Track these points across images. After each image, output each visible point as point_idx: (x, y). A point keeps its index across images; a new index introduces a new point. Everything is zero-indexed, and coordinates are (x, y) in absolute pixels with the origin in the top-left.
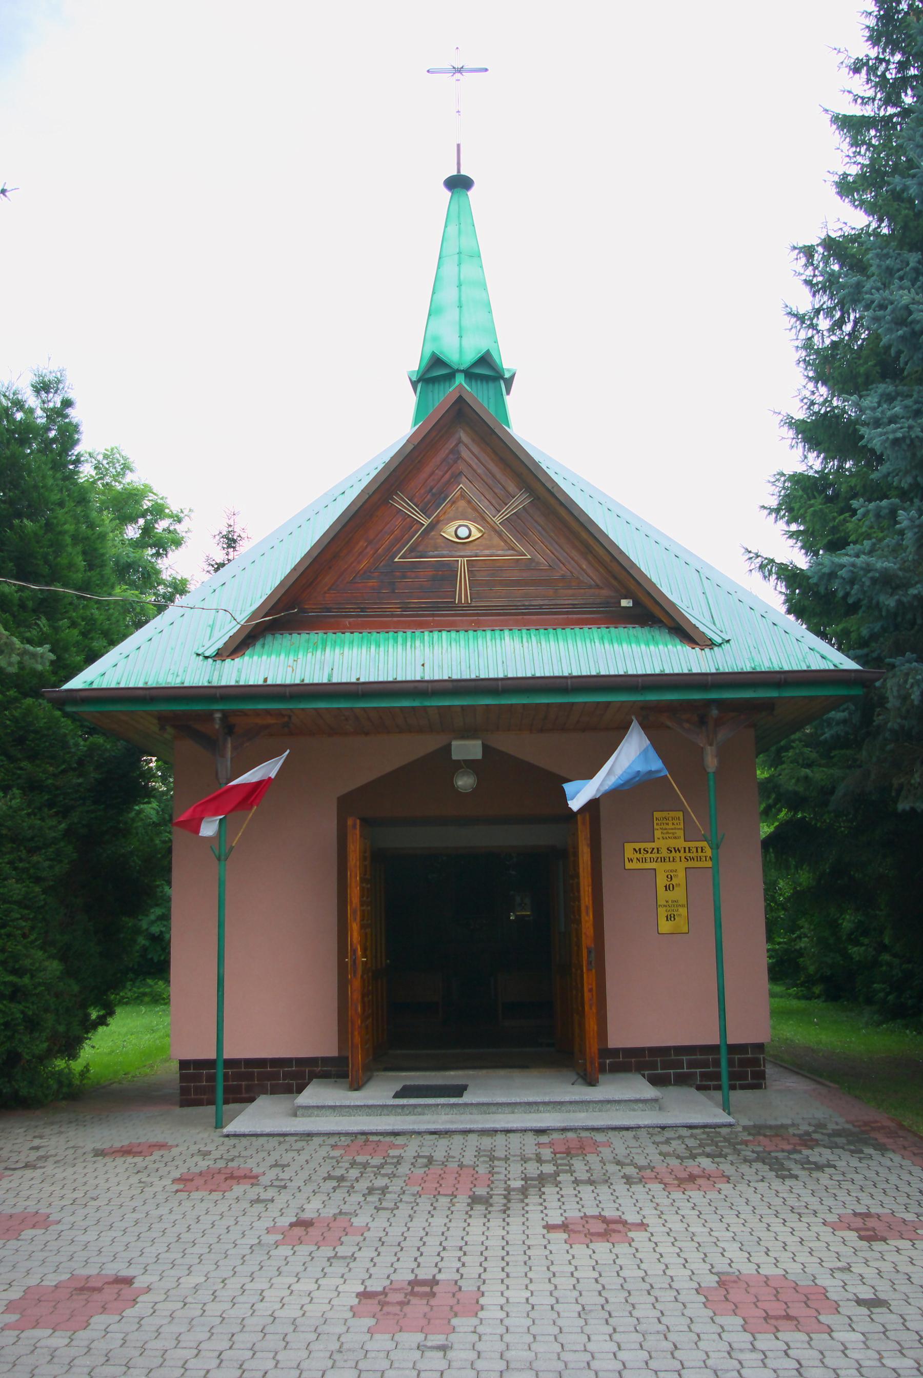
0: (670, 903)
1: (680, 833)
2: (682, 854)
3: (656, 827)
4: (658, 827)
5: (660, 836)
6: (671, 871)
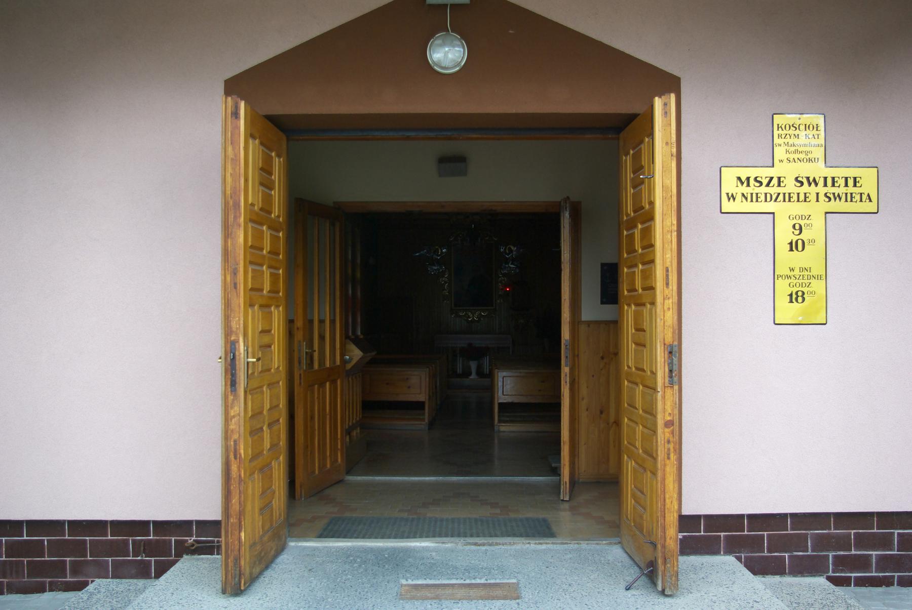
0: (797, 272)
1: (819, 153)
2: (821, 189)
3: (776, 141)
4: (781, 141)
5: (784, 156)
6: (801, 217)
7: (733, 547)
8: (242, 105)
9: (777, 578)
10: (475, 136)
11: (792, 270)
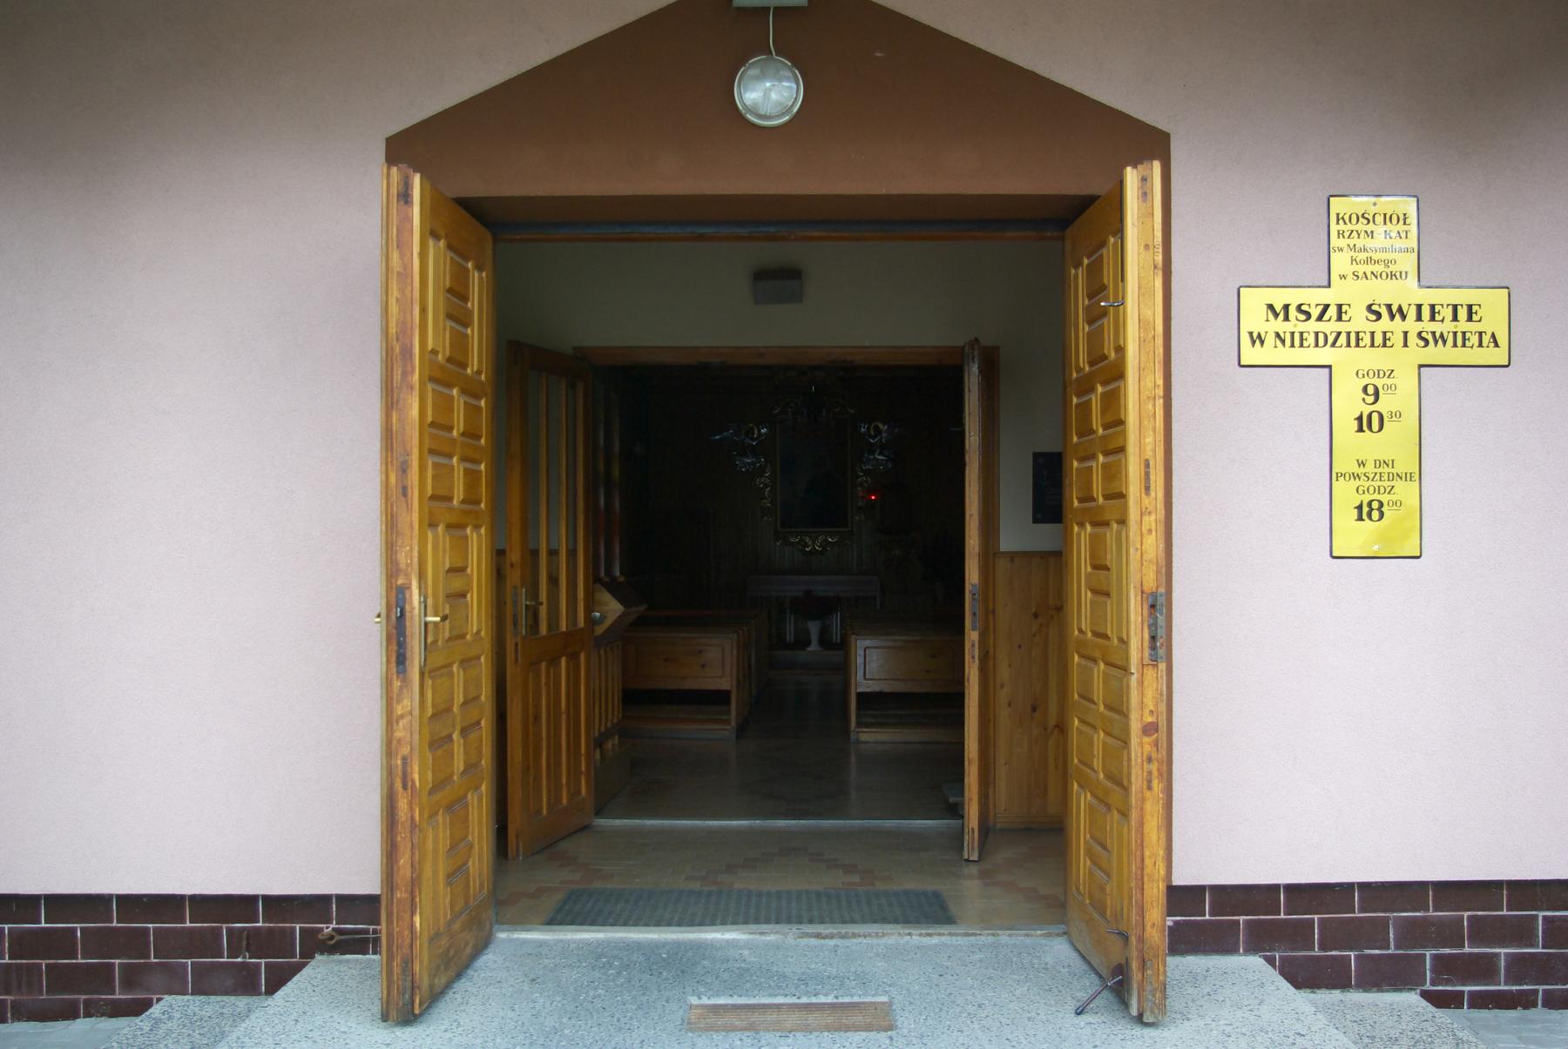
0: (1370, 468)
1: (1408, 263)
2: (1411, 325)
3: (1335, 242)
4: (1342, 243)
5: (1348, 269)
6: (1377, 374)
7: (1260, 940)
8: (417, 180)
9: (1336, 995)
10: (816, 234)
11: (1362, 464)
